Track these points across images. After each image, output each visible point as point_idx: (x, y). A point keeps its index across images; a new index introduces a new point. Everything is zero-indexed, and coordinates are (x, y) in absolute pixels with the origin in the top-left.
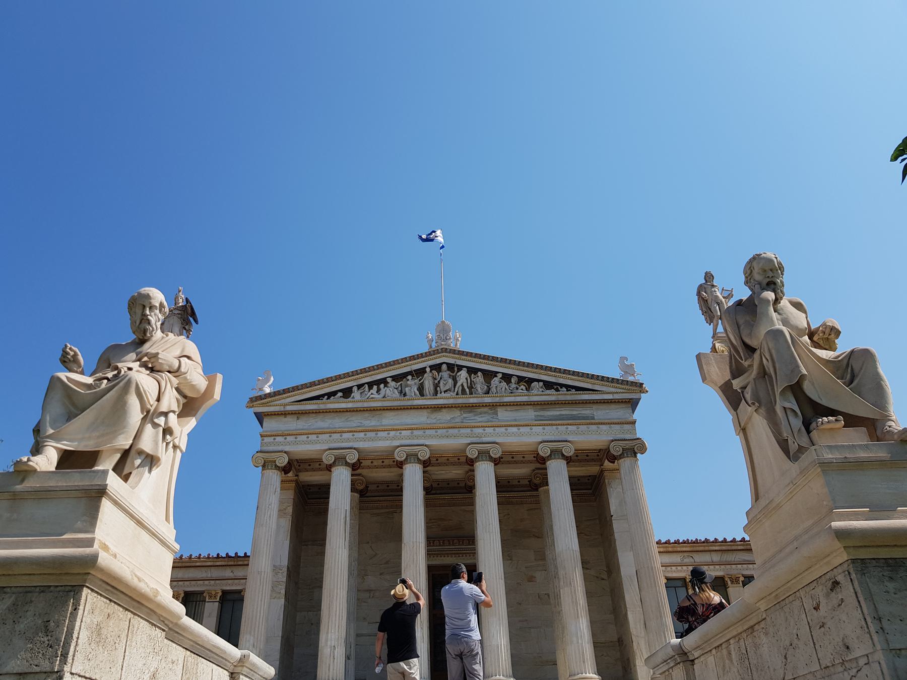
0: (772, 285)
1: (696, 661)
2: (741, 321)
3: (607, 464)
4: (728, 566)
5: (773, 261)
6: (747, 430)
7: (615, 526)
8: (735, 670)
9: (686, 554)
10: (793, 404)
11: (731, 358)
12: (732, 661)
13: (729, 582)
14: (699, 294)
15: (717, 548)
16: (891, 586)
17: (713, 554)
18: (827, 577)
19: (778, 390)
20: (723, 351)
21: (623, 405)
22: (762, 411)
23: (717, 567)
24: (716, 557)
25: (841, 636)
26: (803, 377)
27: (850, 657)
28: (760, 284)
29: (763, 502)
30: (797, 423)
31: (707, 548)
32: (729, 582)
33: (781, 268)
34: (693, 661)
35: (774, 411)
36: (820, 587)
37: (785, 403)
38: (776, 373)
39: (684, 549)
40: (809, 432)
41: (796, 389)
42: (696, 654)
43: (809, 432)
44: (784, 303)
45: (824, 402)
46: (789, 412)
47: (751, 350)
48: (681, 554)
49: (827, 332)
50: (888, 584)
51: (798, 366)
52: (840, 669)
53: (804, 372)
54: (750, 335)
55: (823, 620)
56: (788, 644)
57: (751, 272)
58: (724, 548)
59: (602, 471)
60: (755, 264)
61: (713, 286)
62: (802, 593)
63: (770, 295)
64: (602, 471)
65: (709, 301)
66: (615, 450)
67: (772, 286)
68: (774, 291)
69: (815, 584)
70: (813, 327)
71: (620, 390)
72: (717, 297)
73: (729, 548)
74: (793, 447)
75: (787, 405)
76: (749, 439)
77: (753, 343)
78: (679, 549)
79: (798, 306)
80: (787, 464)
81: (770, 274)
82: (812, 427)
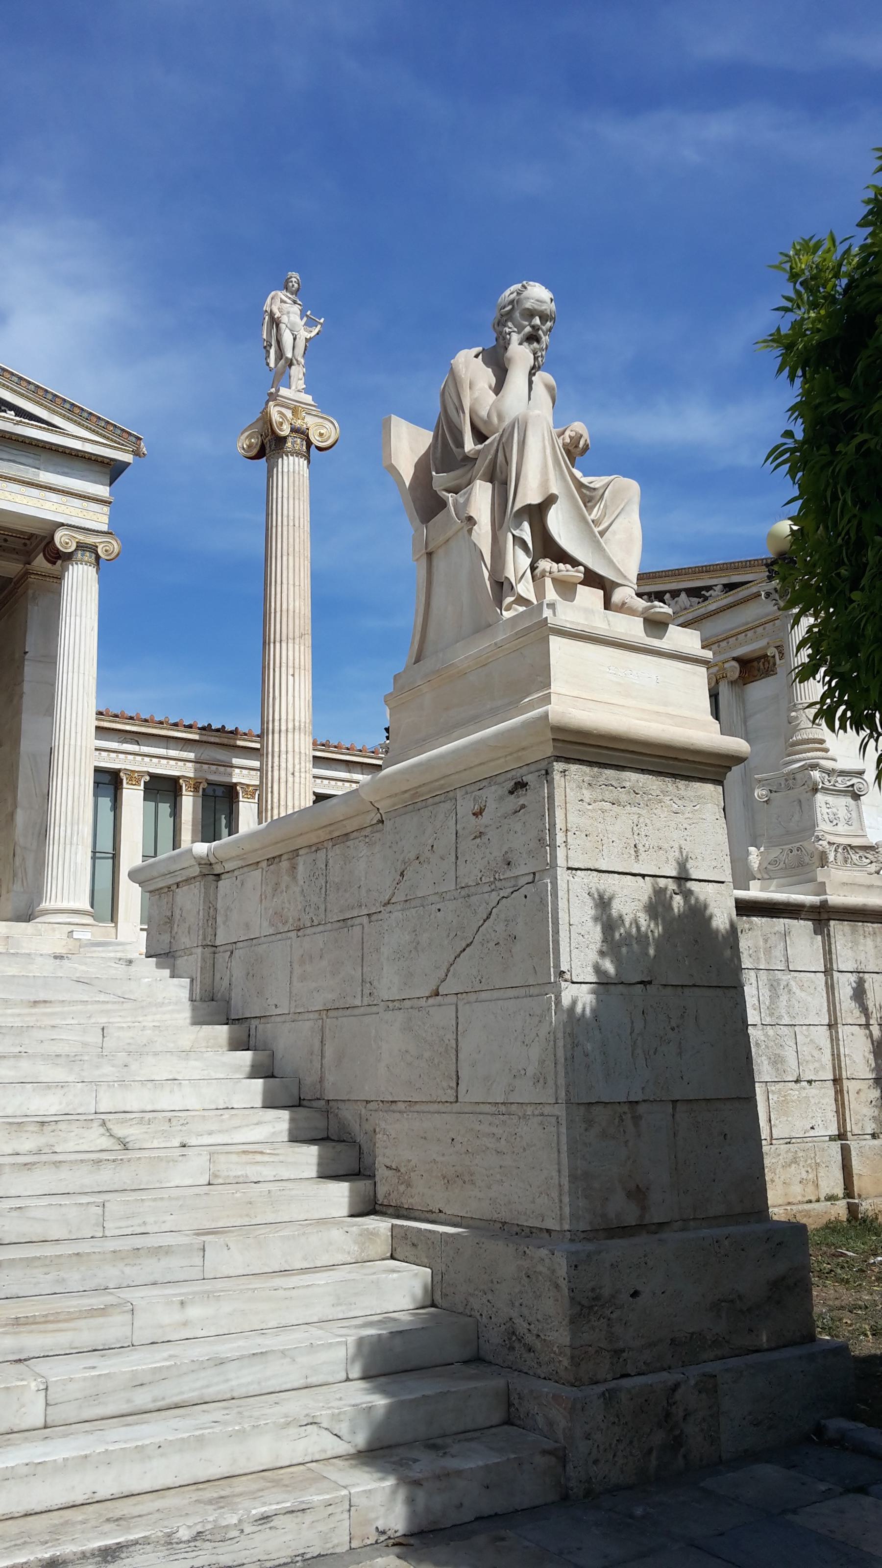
1: (223, 877)
3: (40, 562)
6: (434, 556)
7: (26, 668)
8: (298, 889)
12: (294, 878)
16: (587, 794)
18: (509, 775)
21: (96, 468)
25: (505, 849)
27: (509, 874)
29: (428, 664)
34: (218, 875)
36: (493, 788)
42: (229, 866)
50: (585, 791)
52: (487, 888)
55: (482, 830)
56: (412, 856)
59: (26, 574)
62: (459, 793)
64: (26, 574)
66: (61, 539)
69: (485, 783)
71: (105, 442)
76: (434, 570)
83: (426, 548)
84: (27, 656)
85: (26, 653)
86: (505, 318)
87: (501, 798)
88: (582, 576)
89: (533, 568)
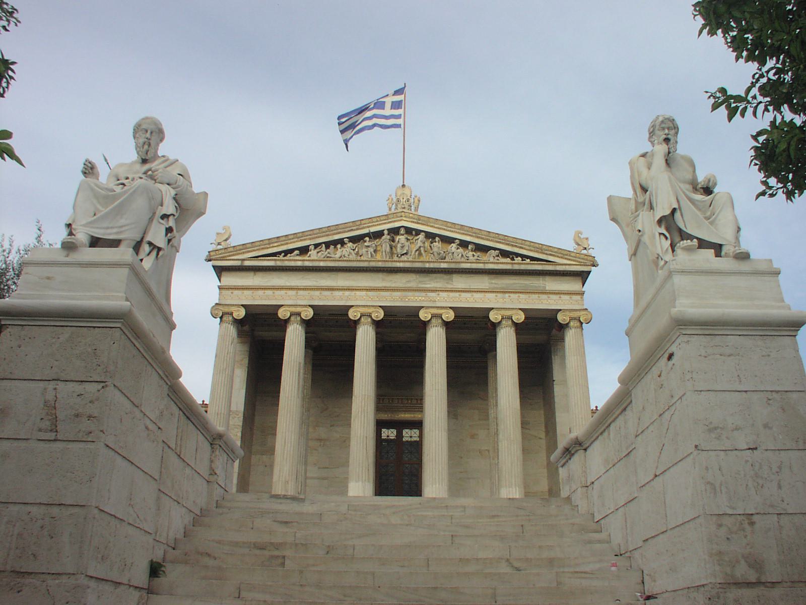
71: (574, 263)
84: (555, 383)
85: (554, 381)
87: (666, 365)
89: (673, 246)
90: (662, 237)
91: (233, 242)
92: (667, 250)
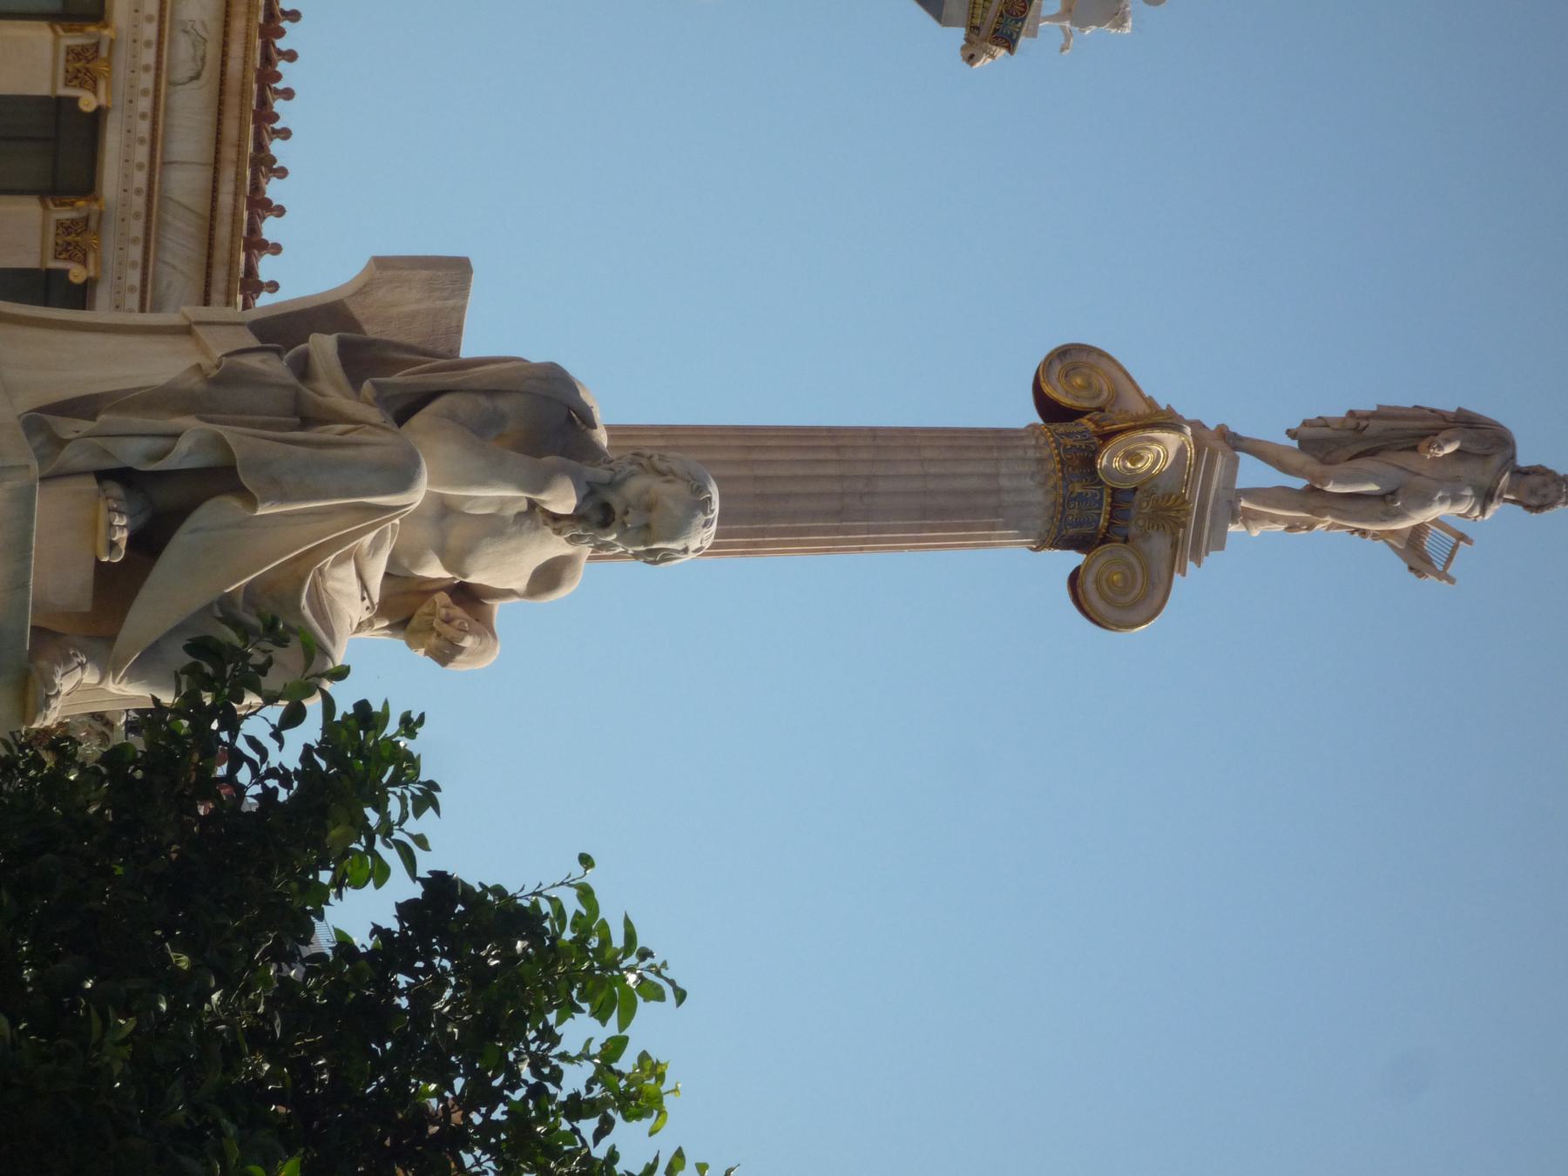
0: (598, 515)
2: (504, 404)
4: (137, 229)
5: (672, 539)
9: (212, 51)
10: (183, 455)
11: (425, 354)
13: (66, 214)
14: (1465, 422)
15: (226, 199)
17: (201, 178)
19: (229, 433)
20: (1134, 456)
22: (196, 383)
23: (140, 179)
24: (185, 183)
26: (251, 501)
28: (613, 485)
30: (132, 453)
31: (229, 153)
32: (66, 214)
33: (655, 557)
35: (185, 412)
37: (191, 441)
38: (275, 440)
39: (236, 50)
40: (102, 476)
41: (220, 478)
43: (102, 476)
44: (555, 547)
45: (182, 541)
46: (161, 443)
47: (405, 409)
48: (214, 27)
49: (449, 631)
51: (284, 498)
53: (262, 511)
54: (452, 416)
57: (660, 473)
58: (223, 231)
60: (679, 488)
61: (1486, 497)
63: (563, 500)
65: (1408, 459)
67: (597, 517)
68: (577, 518)
70: (498, 607)
72: (1425, 501)
73: (221, 254)
74: (68, 428)
75: (184, 445)
77: (417, 421)
78: (238, 25)
79: (548, 578)
80: (26, 402)
81: (632, 520)
82: (115, 490)
83: (199, 323)
86: (644, 462)
88: (105, 559)
90: (161, 443)
91: (1177, 576)
92: (106, 453)
